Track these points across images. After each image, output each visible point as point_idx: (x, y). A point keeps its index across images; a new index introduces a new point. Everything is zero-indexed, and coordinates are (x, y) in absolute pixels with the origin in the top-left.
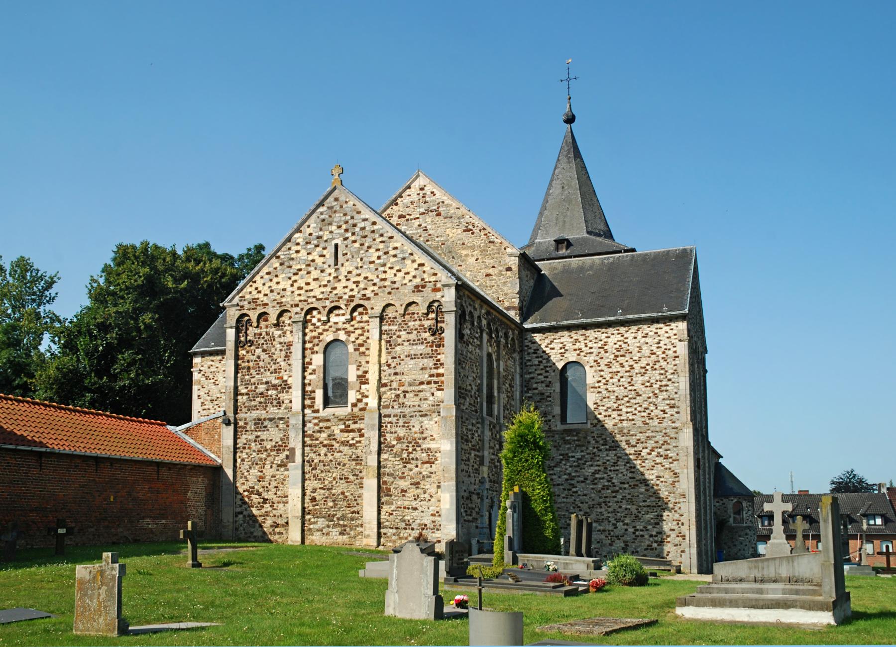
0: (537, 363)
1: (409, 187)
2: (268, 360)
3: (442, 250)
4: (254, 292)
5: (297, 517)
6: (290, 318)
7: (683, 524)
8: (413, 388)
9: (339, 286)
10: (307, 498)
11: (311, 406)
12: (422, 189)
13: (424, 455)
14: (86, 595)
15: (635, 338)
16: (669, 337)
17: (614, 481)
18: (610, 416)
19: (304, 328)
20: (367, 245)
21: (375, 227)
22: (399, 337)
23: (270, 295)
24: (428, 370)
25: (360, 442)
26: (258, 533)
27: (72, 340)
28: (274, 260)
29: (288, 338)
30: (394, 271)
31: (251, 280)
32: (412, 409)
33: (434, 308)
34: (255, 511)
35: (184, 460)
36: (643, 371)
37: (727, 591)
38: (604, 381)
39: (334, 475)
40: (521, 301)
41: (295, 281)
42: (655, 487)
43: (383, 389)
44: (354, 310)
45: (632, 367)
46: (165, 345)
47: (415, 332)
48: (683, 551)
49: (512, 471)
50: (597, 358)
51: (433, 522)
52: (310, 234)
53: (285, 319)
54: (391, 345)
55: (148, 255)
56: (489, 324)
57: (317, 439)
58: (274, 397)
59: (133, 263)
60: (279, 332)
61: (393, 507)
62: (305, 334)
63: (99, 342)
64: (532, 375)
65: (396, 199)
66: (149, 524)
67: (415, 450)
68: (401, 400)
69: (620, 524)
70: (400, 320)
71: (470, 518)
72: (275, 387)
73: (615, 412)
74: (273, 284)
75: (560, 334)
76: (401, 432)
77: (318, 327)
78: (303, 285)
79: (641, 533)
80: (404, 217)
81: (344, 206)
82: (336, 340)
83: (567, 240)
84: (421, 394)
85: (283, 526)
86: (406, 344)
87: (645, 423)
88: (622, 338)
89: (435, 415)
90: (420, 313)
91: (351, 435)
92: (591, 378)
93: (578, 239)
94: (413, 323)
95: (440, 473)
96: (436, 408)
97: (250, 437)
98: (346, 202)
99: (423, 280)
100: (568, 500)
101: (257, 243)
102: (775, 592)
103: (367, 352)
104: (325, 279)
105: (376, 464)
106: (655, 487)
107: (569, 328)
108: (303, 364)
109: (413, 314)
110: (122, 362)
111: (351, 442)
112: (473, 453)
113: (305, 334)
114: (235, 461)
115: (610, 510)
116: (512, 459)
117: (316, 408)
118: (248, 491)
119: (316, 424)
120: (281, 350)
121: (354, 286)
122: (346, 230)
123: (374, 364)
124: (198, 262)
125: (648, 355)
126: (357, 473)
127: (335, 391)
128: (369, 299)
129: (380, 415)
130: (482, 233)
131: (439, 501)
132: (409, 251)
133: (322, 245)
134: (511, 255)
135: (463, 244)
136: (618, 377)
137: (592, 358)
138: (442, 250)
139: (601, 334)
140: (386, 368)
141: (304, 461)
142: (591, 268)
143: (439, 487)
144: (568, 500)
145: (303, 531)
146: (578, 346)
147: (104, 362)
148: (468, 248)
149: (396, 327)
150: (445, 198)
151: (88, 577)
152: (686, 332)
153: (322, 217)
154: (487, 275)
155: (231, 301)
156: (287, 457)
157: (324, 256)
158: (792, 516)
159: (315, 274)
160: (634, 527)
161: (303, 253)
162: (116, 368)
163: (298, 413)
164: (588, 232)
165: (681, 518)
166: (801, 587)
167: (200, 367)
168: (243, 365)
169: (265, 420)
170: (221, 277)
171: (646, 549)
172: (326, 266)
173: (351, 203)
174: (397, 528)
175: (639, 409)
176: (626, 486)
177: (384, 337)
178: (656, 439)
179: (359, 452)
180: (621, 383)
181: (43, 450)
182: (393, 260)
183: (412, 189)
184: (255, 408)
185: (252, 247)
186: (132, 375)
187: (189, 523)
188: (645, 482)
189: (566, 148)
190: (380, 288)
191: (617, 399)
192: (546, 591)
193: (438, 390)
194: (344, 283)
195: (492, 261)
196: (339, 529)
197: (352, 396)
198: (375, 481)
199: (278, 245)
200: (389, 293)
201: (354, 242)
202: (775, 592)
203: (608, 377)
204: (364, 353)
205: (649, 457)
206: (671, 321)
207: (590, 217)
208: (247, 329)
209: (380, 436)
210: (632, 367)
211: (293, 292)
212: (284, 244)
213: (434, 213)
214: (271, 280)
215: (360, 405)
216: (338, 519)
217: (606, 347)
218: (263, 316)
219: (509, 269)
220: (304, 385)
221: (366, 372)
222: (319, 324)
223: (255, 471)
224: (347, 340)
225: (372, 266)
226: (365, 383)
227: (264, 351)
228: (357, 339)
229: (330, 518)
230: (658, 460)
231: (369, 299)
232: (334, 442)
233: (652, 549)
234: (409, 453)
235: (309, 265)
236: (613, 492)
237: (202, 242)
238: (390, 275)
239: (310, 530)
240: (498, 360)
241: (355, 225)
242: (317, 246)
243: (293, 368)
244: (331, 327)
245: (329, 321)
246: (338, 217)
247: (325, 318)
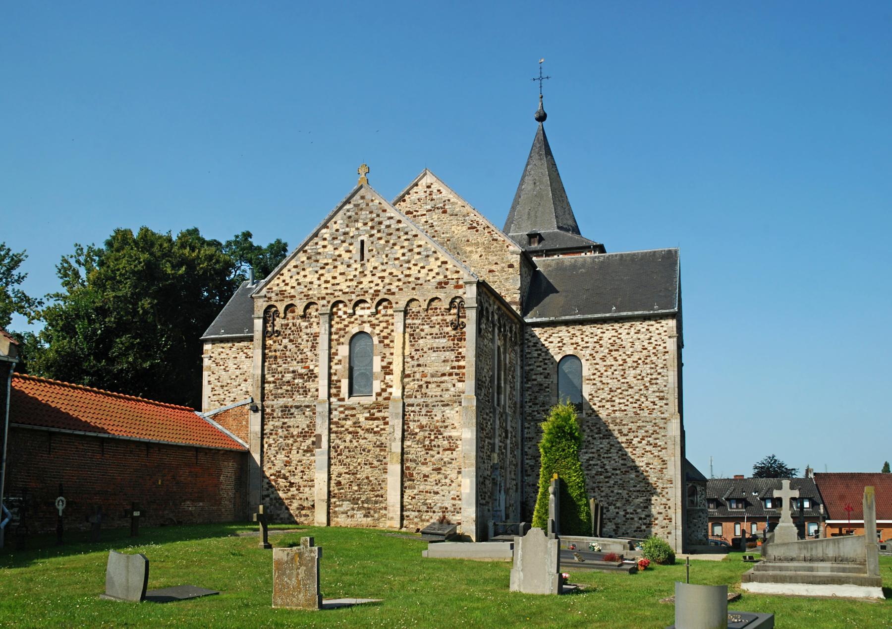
0: (536, 355)
1: (416, 185)
2: (294, 349)
3: (448, 246)
4: (282, 285)
5: (323, 500)
6: (317, 310)
7: (669, 508)
8: (435, 379)
9: (366, 280)
10: (333, 482)
11: (337, 395)
12: (429, 187)
13: (446, 442)
14: (284, 574)
15: (628, 334)
16: (659, 334)
17: (607, 467)
18: (603, 406)
19: (331, 320)
20: (392, 242)
21: (400, 225)
22: (422, 330)
23: (297, 287)
24: (450, 363)
25: (384, 429)
26: (284, 515)
27: (69, 323)
28: (301, 254)
29: (315, 329)
30: (418, 268)
31: (278, 273)
32: (434, 399)
33: (457, 304)
34: (281, 494)
35: (218, 445)
36: (635, 364)
37: (781, 569)
38: (599, 374)
39: (359, 460)
40: (522, 297)
41: (322, 275)
42: (645, 474)
43: (406, 380)
44: (379, 304)
45: (625, 361)
46: (162, 330)
47: (437, 326)
48: (669, 533)
49: (550, 460)
50: (593, 352)
51: (454, 505)
52: (337, 230)
53: (312, 311)
54: (414, 338)
55: (147, 240)
56: (499, 319)
57: (343, 427)
58: (300, 385)
59: (132, 249)
60: (306, 324)
61: (416, 491)
62: (331, 326)
63: (97, 325)
64: (531, 367)
65: (404, 196)
66: (189, 506)
67: (437, 437)
68: (424, 391)
69: (612, 508)
70: (423, 314)
71: (484, 502)
72: (301, 376)
73: (609, 403)
75: (558, 328)
76: (424, 421)
77: (344, 320)
78: (330, 279)
80: (412, 213)
81: (371, 204)
82: (361, 332)
83: (539, 234)
84: (442, 385)
85: (309, 508)
86: (429, 337)
87: (636, 414)
88: (616, 334)
90: (443, 308)
91: (376, 423)
92: (587, 370)
93: (549, 234)
94: (435, 318)
95: (460, 460)
96: (457, 399)
97: (276, 424)
98: (372, 201)
99: (446, 277)
101: (244, 230)
102: (824, 569)
103: (391, 344)
104: (351, 274)
105: (400, 451)
106: (645, 474)
107: (567, 323)
108: (330, 354)
109: (436, 309)
110: (120, 346)
111: (375, 429)
112: (487, 440)
113: (331, 326)
114: (262, 446)
115: (603, 494)
116: (550, 448)
117: (341, 396)
118: (275, 475)
119: (341, 412)
120: (307, 341)
121: (379, 281)
122: (372, 228)
123: (398, 356)
124: (193, 249)
125: (640, 350)
126: (381, 458)
127: (357, 378)
128: (393, 294)
129: (404, 404)
130: (486, 231)
131: (460, 486)
132: (433, 249)
133: (349, 241)
134: (513, 253)
135: (468, 241)
136: (612, 370)
137: (588, 351)
138: (448, 246)
139: (596, 330)
140: (409, 360)
141: (329, 447)
142: (583, 265)
143: (459, 473)
145: (328, 513)
146: (575, 340)
147: (102, 346)
148: (472, 245)
149: (420, 321)
150: (451, 196)
151: (285, 559)
152: (675, 329)
154: (490, 271)
155: (258, 292)
156: (313, 443)
157: (350, 251)
158: (801, 500)
159: (342, 268)
161: (330, 248)
162: (114, 352)
163: (324, 401)
164: (559, 228)
165: (668, 502)
166: (847, 566)
167: (210, 354)
168: (270, 354)
169: (291, 407)
170: (215, 264)
171: (635, 531)
172: (352, 261)
173: (377, 201)
174: (419, 511)
175: (631, 400)
176: (618, 472)
177: (408, 330)
178: (646, 429)
179: (383, 439)
180: (614, 376)
181: (106, 436)
183: (420, 187)
184: (283, 396)
185: (240, 234)
186: (131, 359)
187: (261, 507)
188: (636, 468)
189: (538, 145)
190: (404, 283)
192: (612, 569)
193: (459, 381)
194: (370, 277)
195: (495, 258)
196: (364, 512)
197: (377, 386)
198: (399, 466)
199: (306, 239)
200: (414, 289)
201: (380, 239)
202: (824, 569)
203: (602, 370)
204: (388, 345)
205: (639, 445)
206: (661, 319)
207: (560, 213)
208: (274, 320)
209: (403, 425)
210: (625, 361)
211: (319, 285)
212: (311, 239)
213: (441, 211)
214: (298, 273)
215: (385, 395)
216: (363, 502)
217: (601, 342)
218: (290, 308)
219: (511, 266)
220: (330, 375)
221: (390, 363)
222: (344, 316)
223: (281, 456)
224: (372, 332)
225: (397, 262)
226: (389, 374)
227: (291, 341)
228: (382, 331)
229: (354, 501)
230: (648, 448)
231: (393, 294)
232: (359, 430)
233: (641, 531)
234: (431, 440)
235: (335, 260)
236: (606, 477)
237: (191, 228)
238: (414, 271)
239: (335, 512)
240: (505, 353)
241: (380, 223)
242: (343, 242)
243: (321, 358)
244: (356, 319)
245: (354, 314)
246: (364, 214)
247: (351, 311)
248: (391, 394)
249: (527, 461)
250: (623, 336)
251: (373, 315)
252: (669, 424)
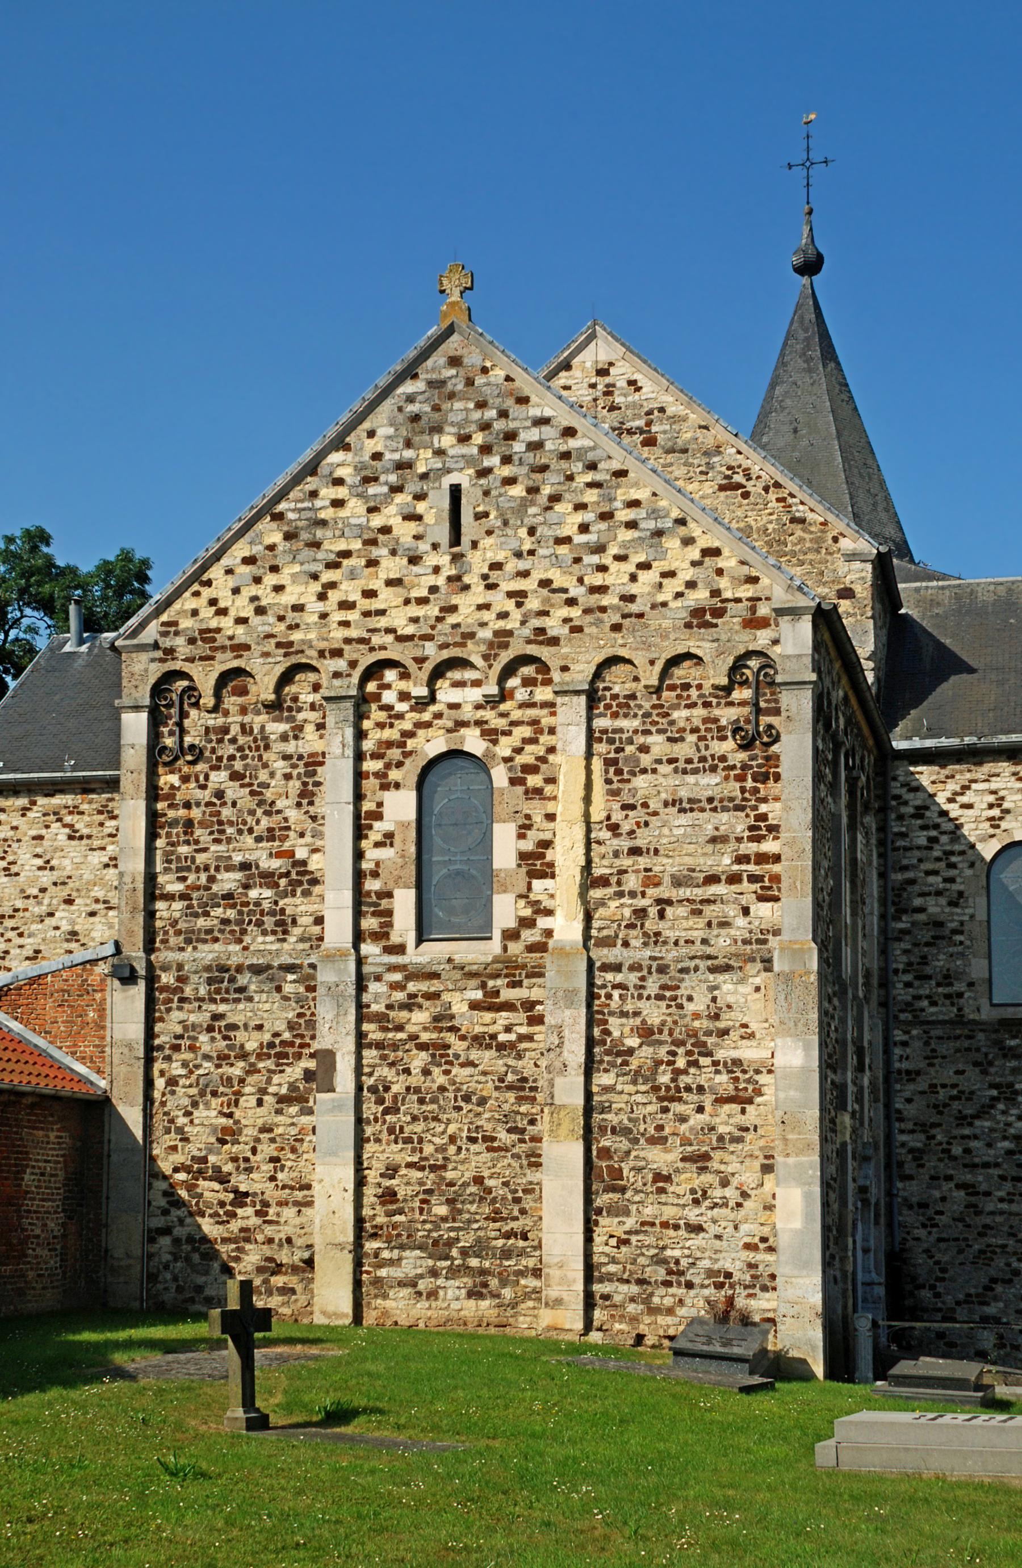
0: (923, 841)
2: (246, 801)
20: (547, 490)
21: (573, 443)
22: (644, 749)
30: (630, 567)
32: (684, 950)
78: (355, 596)
86: (665, 769)
122: (486, 449)
182: (626, 535)
183: (576, 372)
215: (530, 936)
232: (451, 1038)
241: (511, 436)
248: (549, 933)
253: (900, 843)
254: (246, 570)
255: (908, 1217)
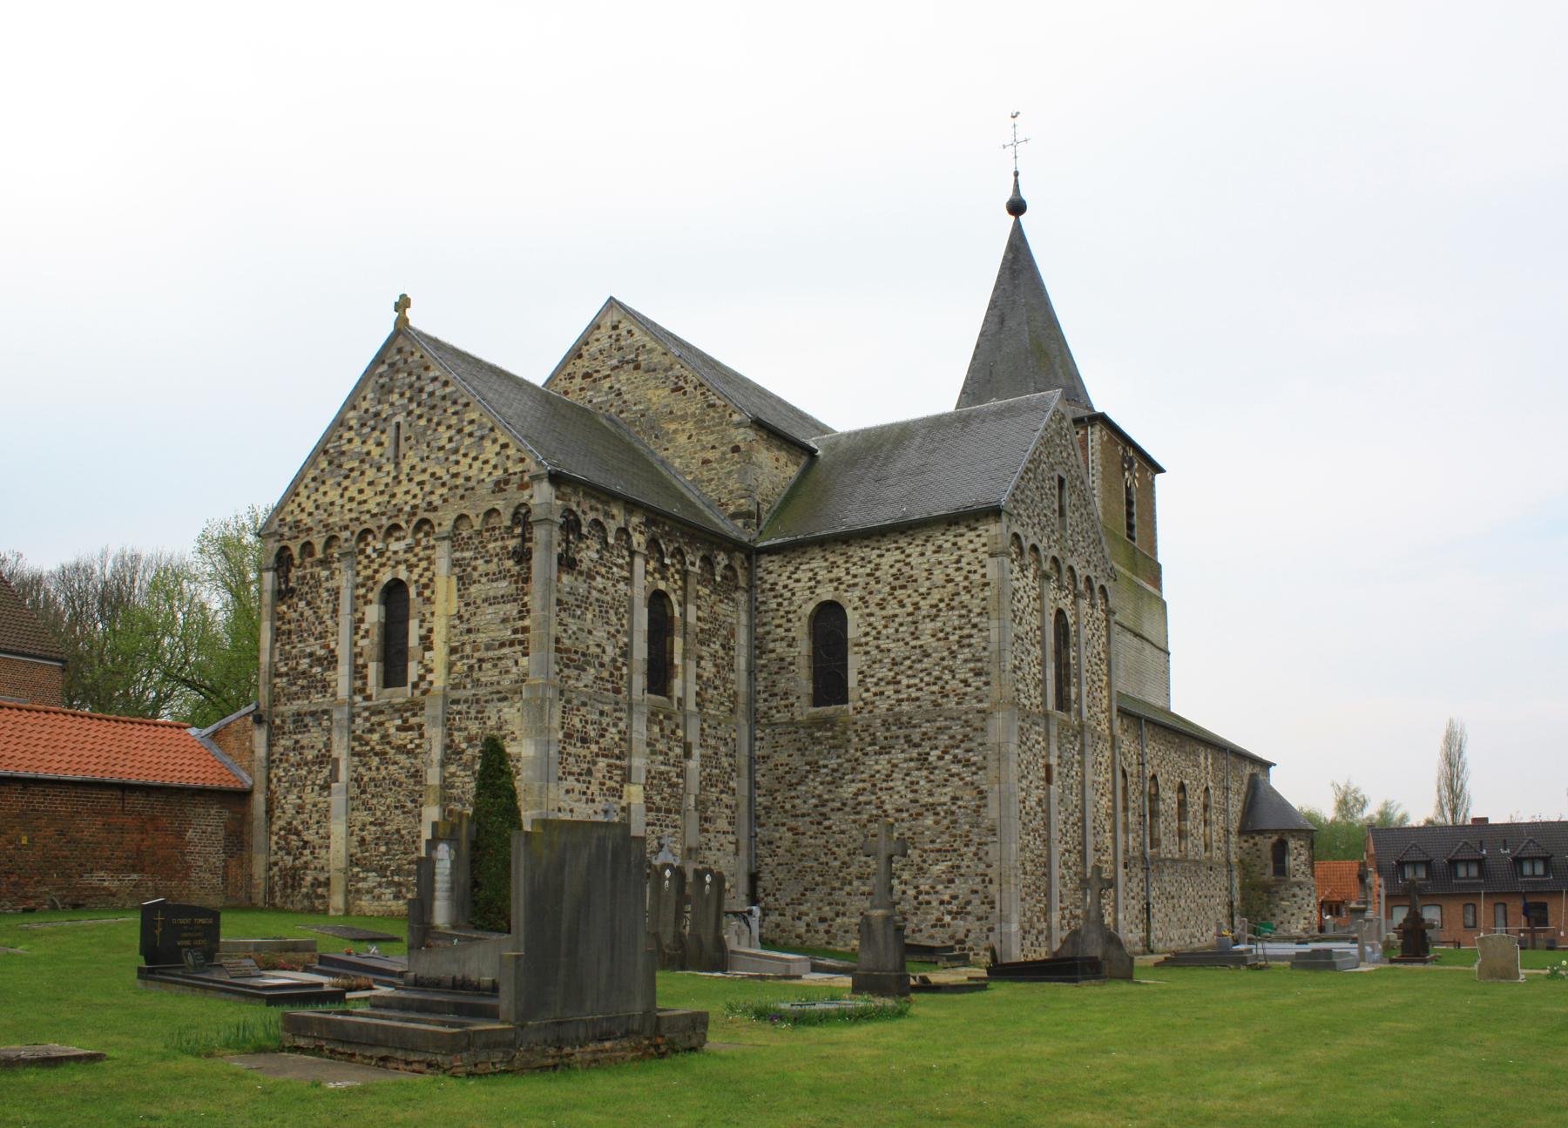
0: (774, 606)
2: (312, 618)
4: (297, 511)
7: (991, 881)
8: (490, 654)
9: (399, 490)
12: (615, 328)
15: (922, 554)
16: (974, 551)
17: (887, 807)
18: (882, 693)
20: (435, 420)
21: (448, 390)
22: (475, 569)
30: (469, 460)
32: (490, 689)
45: (916, 606)
47: (495, 560)
50: (864, 593)
56: (653, 543)
68: (475, 675)
72: (319, 661)
74: (318, 496)
76: (474, 728)
78: (355, 494)
79: (927, 897)
86: (484, 580)
87: (936, 704)
88: (902, 557)
89: (517, 697)
100: (818, 842)
122: (411, 400)
134: (739, 425)
137: (857, 592)
144: (818, 842)
153: (381, 381)
160: (916, 887)
165: (989, 871)
171: (934, 926)
175: (926, 679)
176: (905, 815)
182: (468, 441)
183: (603, 330)
191: (894, 663)
200: (462, 497)
203: (879, 624)
205: (941, 763)
210: (916, 606)
215: (424, 685)
217: (878, 574)
224: (409, 579)
230: (955, 768)
232: (388, 748)
233: (943, 926)
235: (362, 461)
241: (421, 390)
242: (373, 429)
248: (431, 683)
249: (759, 800)
250: (914, 560)
251: (409, 549)
252: (991, 721)
253: (763, 608)
254: (312, 485)
255: (762, 851)
